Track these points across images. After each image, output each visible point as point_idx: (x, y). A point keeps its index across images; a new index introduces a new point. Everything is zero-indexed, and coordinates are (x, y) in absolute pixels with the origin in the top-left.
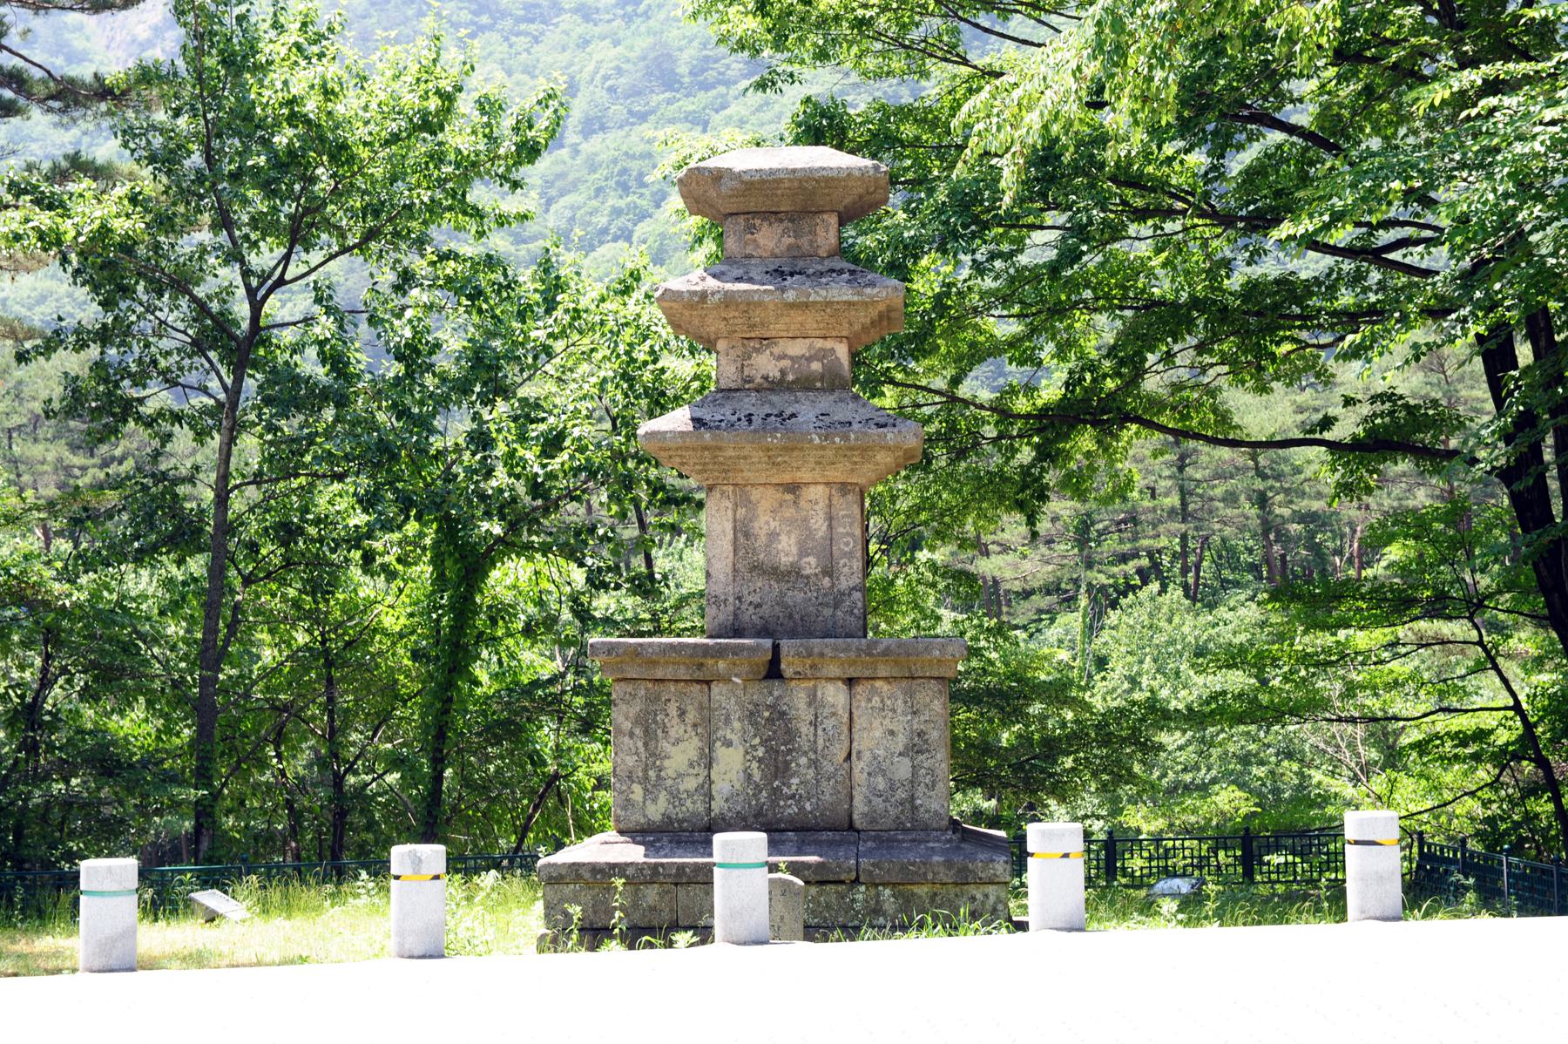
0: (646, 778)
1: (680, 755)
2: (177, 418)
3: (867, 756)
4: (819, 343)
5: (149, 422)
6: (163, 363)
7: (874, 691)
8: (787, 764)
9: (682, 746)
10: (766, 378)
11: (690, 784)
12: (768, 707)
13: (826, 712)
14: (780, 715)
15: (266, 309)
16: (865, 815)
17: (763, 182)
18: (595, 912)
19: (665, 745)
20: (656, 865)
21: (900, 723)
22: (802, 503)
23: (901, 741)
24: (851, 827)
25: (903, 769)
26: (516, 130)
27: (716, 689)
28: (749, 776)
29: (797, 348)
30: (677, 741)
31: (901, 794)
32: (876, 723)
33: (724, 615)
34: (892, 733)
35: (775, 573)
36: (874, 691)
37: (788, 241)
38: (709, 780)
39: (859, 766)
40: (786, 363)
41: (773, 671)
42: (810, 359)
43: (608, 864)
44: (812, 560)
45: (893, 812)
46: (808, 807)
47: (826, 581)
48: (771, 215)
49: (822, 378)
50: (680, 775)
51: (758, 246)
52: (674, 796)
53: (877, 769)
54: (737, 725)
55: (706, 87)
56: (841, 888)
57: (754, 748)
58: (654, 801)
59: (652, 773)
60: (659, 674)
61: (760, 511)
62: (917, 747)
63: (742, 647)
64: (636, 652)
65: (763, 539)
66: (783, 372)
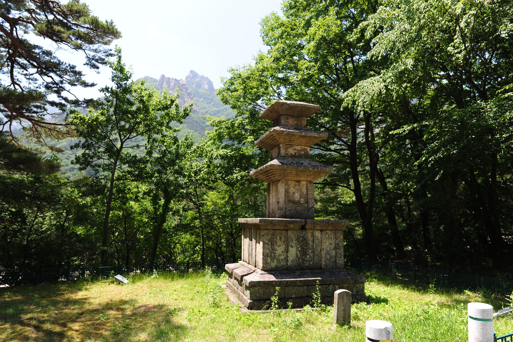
0: (271, 256)
3: (325, 250)
4: (303, 147)
5: (93, 167)
6: (98, 154)
7: (327, 233)
9: (280, 247)
10: (291, 154)
11: (282, 257)
12: (302, 237)
13: (316, 238)
14: (305, 239)
16: (324, 265)
17: (294, 106)
18: (264, 295)
21: (333, 242)
24: (321, 268)
25: (333, 253)
26: (184, 111)
28: (297, 255)
29: (299, 148)
30: (279, 246)
31: (333, 260)
32: (327, 241)
33: (282, 213)
34: (331, 244)
36: (327, 233)
38: (287, 256)
39: (323, 252)
40: (296, 151)
41: (303, 228)
42: (301, 151)
43: (268, 281)
44: (303, 199)
46: (311, 263)
48: (292, 116)
49: (304, 155)
50: (280, 255)
52: (278, 261)
53: (327, 253)
54: (294, 242)
55: (136, 142)
56: (326, 286)
57: (298, 248)
58: (273, 262)
60: (276, 228)
62: (336, 248)
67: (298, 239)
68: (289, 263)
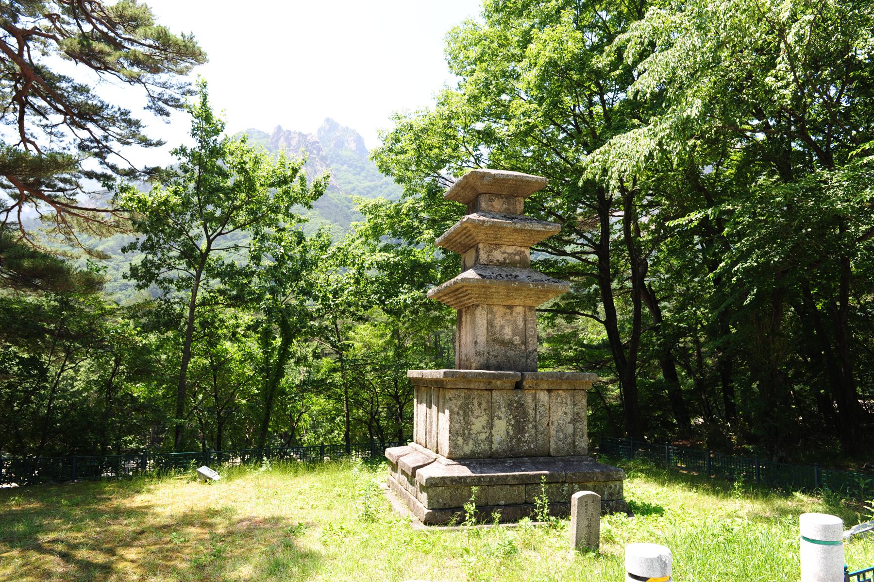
1: (478, 423)
2: (171, 281)
3: (556, 423)
4: (519, 249)
7: (559, 395)
8: (524, 427)
10: (498, 261)
11: (483, 436)
13: (540, 404)
14: (521, 405)
15: (213, 243)
16: (555, 449)
17: (503, 179)
19: (472, 419)
20: (480, 477)
21: (569, 409)
22: (514, 314)
23: (570, 416)
24: (549, 455)
25: (570, 429)
27: (495, 393)
28: (508, 433)
29: (510, 250)
30: (478, 417)
31: (569, 440)
32: (559, 409)
33: (483, 360)
34: (566, 413)
35: (503, 343)
36: (559, 395)
37: (505, 206)
38: (491, 435)
39: (553, 428)
40: (506, 255)
41: (518, 386)
42: (515, 255)
44: (517, 338)
45: (566, 448)
47: (523, 347)
48: (499, 196)
49: (520, 263)
50: (478, 433)
51: (493, 207)
53: (560, 429)
54: (503, 410)
56: (558, 485)
57: (510, 420)
58: (467, 444)
59: (466, 432)
60: (472, 386)
61: (497, 316)
62: (575, 420)
63: (509, 375)
64: (464, 376)
65: (498, 328)
66: (505, 259)
67: (509, 406)
68: (495, 446)
